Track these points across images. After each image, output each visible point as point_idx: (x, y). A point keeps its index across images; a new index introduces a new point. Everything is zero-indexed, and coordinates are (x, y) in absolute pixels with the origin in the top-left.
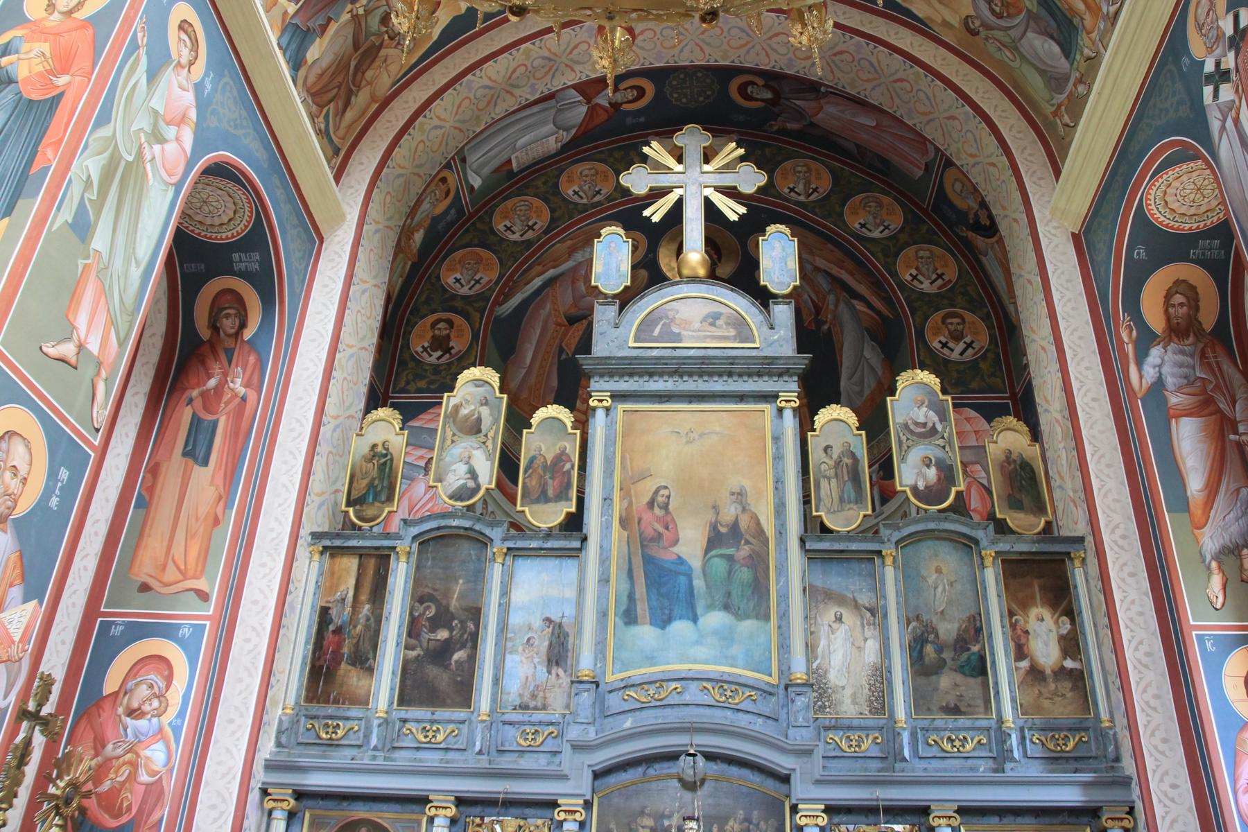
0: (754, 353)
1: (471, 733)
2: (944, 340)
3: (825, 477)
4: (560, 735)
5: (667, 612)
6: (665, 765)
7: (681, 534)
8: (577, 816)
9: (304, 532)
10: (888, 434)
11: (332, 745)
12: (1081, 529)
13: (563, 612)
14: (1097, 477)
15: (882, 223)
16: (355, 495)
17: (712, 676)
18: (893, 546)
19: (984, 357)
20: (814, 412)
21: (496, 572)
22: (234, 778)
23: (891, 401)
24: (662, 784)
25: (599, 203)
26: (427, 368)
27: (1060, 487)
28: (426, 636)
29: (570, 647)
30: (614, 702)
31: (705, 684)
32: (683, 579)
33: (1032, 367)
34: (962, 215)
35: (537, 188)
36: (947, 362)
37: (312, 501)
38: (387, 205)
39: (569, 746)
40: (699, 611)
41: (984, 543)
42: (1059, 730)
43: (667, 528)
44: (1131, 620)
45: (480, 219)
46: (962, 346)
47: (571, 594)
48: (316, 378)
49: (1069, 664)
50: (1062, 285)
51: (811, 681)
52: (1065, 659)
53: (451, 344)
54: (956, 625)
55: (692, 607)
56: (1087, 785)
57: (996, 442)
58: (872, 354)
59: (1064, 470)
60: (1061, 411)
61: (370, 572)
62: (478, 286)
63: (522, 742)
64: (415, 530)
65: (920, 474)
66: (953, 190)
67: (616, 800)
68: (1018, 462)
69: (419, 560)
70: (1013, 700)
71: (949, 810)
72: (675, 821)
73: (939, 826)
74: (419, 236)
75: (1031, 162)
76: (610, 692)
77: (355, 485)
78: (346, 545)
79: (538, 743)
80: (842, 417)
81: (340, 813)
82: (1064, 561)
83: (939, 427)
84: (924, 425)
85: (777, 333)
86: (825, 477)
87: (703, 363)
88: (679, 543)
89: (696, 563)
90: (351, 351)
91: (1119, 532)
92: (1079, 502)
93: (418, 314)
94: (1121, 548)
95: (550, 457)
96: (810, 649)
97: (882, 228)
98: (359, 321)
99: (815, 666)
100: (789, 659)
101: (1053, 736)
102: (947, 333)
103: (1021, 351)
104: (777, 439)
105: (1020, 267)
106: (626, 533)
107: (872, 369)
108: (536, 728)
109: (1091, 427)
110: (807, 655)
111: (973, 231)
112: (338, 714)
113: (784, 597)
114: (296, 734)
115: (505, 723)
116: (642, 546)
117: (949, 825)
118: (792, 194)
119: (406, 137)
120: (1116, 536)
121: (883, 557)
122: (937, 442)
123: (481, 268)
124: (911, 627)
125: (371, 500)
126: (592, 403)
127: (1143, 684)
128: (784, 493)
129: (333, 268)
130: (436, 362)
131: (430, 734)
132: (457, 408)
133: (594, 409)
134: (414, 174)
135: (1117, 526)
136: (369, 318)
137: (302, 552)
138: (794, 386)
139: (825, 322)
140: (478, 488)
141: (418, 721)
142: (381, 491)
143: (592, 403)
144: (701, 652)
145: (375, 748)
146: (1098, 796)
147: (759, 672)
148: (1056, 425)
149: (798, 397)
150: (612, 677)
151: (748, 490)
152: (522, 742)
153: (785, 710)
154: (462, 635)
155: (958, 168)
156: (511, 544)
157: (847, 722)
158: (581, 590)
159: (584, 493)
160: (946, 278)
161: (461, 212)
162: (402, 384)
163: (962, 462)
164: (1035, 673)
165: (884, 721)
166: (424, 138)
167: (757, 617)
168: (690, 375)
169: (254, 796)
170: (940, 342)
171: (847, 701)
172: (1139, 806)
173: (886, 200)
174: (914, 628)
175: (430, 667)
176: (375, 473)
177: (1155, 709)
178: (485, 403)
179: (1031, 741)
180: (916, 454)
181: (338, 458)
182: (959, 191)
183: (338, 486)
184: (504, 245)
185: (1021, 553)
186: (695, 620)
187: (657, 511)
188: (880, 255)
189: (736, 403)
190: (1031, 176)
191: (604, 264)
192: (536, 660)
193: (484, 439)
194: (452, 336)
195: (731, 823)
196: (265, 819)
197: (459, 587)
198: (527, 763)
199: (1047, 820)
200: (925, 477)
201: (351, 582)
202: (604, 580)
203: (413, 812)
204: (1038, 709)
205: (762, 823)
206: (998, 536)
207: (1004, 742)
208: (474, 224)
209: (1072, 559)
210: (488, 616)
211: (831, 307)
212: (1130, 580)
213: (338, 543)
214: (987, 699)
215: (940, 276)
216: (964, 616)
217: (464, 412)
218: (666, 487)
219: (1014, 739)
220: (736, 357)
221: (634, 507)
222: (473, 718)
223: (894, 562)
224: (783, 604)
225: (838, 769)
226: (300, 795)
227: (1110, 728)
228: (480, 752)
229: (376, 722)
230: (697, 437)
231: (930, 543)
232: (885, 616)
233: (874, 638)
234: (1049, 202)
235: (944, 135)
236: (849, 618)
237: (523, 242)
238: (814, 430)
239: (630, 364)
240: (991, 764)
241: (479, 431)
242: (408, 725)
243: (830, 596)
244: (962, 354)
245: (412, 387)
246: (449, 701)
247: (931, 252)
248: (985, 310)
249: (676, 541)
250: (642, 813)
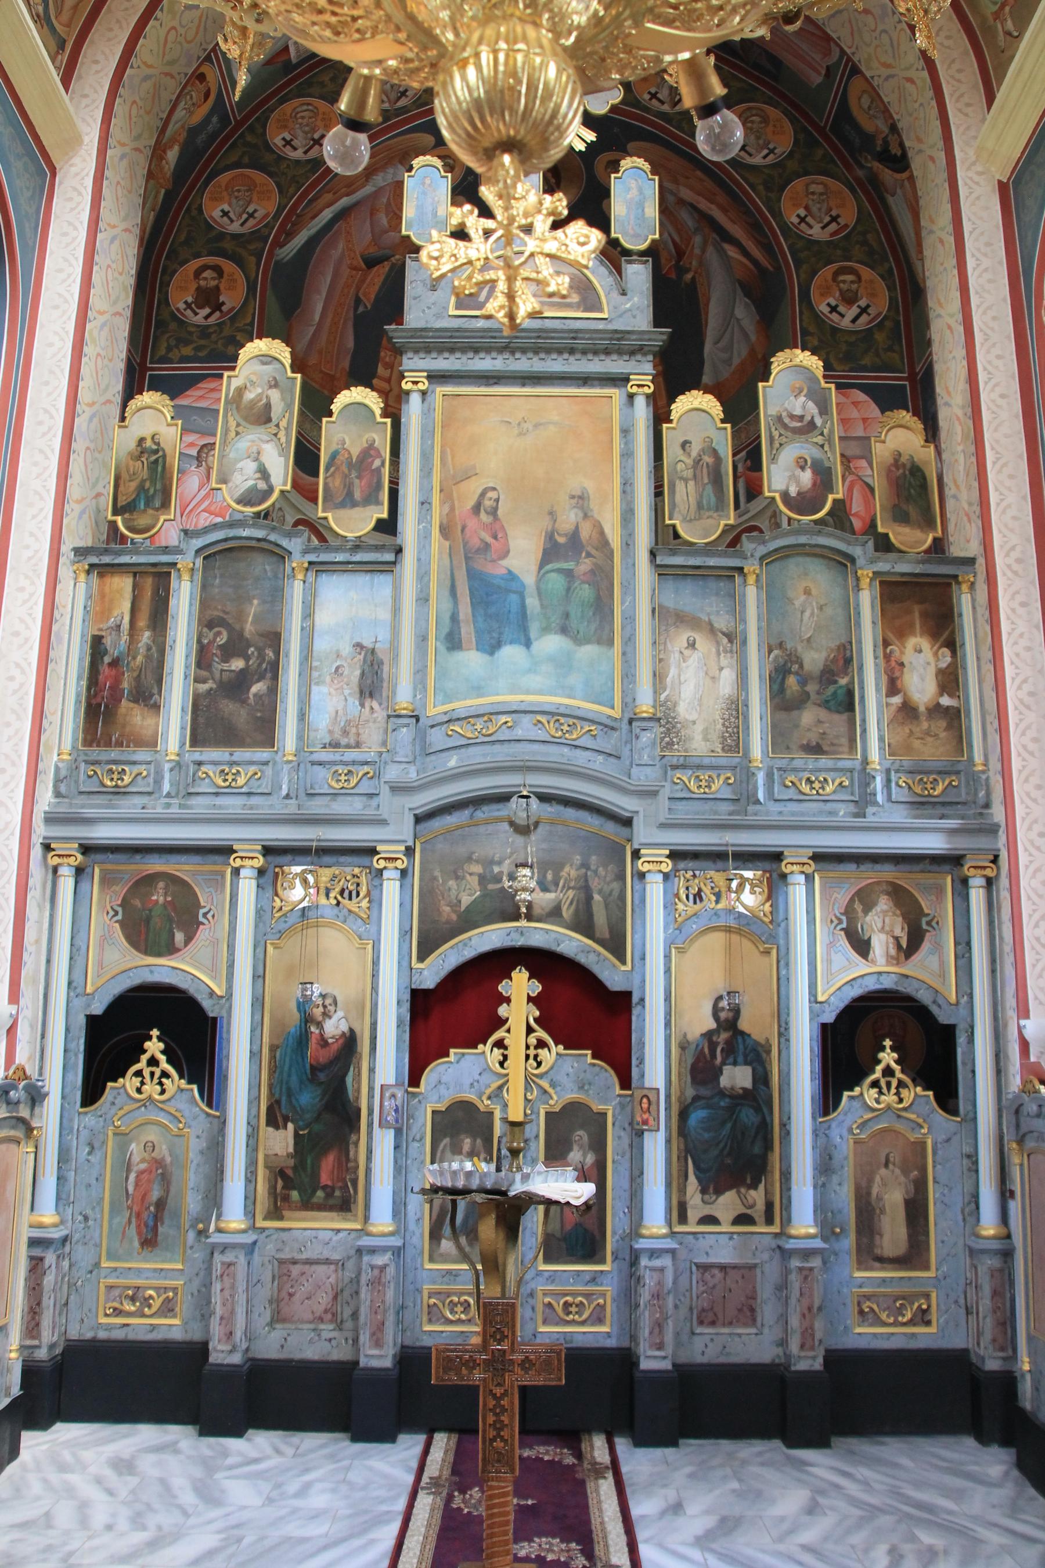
0: (601, 326)
1: (277, 774)
2: (833, 303)
3: (681, 478)
4: (377, 776)
5: (495, 635)
6: (495, 806)
7: (513, 544)
8: (399, 864)
9: (66, 548)
10: (758, 414)
11: (118, 792)
12: (972, 548)
13: (378, 636)
14: (997, 490)
15: (766, 145)
16: (122, 501)
17: (546, 708)
18: (757, 562)
19: (880, 326)
20: (672, 400)
21: (296, 590)
22: (12, 834)
23: (764, 387)
24: (490, 828)
25: (404, 110)
26: (192, 329)
27: (955, 497)
28: (218, 666)
29: (385, 676)
30: (437, 738)
31: (539, 717)
32: (514, 598)
33: (935, 348)
34: (868, 139)
35: (322, 84)
36: (835, 330)
37: (72, 510)
38: (134, 119)
39: (387, 788)
40: (533, 634)
41: (861, 562)
42: (928, 773)
43: (495, 537)
44: (1017, 655)
45: (251, 129)
46: (854, 311)
47: (384, 615)
48: (64, 356)
49: (946, 701)
50: (979, 250)
51: (659, 715)
52: (941, 695)
53: (222, 299)
54: (824, 654)
55: (524, 628)
56: (952, 832)
57: (884, 442)
58: (744, 313)
59: (961, 477)
60: (963, 407)
61: (148, 593)
62: (251, 222)
63: (334, 784)
64: (198, 543)
65: (793, 478)
66: (859, 106)
67: (439, 846)
68: (908, 466)
69: (204, 578)
70: (881, 739)
71: (804, 856)
72: (506, 867)
73: (792, 873)
74: (172, 155)
75: (959, 81)
76: (432, 726)
77: (121, 488)
78: (116, 561)
79: (352, 785)
80: (704, 406)
81: (133, 867)
82: (949, 585)
83: (818, 421)
84: (801, 418)
85: (629, 300)
86: (681, 478)
87: (539, 337)
88: (511, 554)
89: (529, 579)
90: (102, 319)
91: (1014, 555)
92: (973, 517)
93: (176, 259)
94: (1016, 573)
95: (355, 452)
96: (658, 677)
97: (766, 152)
98: (110, 278)
99: (663, 697)
100: (634, 691)
101: (921, 779)
102: (837, 294)
103: (924, 323)
104: (625, 432)
105: (932, 221)
106: (447, 544)
107: (746, 335)
108: (350, 768)
109: (996, 430)
110: (654, 684)
111: (879, 161)
112: (123, 758)
113: (630, 619)
114: (77, 782)
115: (313, 763)
116: (467, 559)
117: (802, 872)
118: (654, 101)
119: (152, 23)
120: (1010, 560)
121: (744, 575)
122: (815, 440)
123: (255, 197)
124: (772, 656)
125: (142, 507)
126: (406, 386)
127: (1022, 726)
128: (633, 497)
129: (72, 209)
130: (203, 322)
131: (230, 777)
132: (240, 391)
133: (408, 393)
134: (166, 74)
135: (1013, 548)
136: (121, 274)
137: (65, 572)
138: (649, 367)
139: (688, 270)
140: (271, 490)
141: (215, 763)
142: (153, 496)
143: (406, 386)
144: (535, 681)
145: (168, 795)
146: (961, 844)
147: (599, 704)
148: (957, 423)
149: (652, 381)
150: (434, 710)
151: (590, 492)
152: (334, 784)
153: (629, 746)
154: (260, 665)
155: (866, 79)
156: (312, 557)
157: (697, 761)
158: (396, 611)
159: (397, 484)
160: (842, 221)
161: (225, 119)
162: (162, 351)
163: (842, 455)
164: (908, 711)
165: (737, 760)
166: (175, 23)
167: (599, 642)
168: (524, 351)
169: (37, 852)
170: (829, 305)
171: (698, 737)
172: (1004, 855)
173: (773, 112)
174: (776, 657)
175: (226, 701)
176: (145, 474)
177: (1032, 754)
178: (275, 384)
179: (898, 785)
180: (790, 453)
181: (97, 455)
182: (866, 107)
183: (99, 488)
184: (283, 166)
185: (903, 574)
186: (528, 644)
187: (484, 517)
188: (761, 188)
189: (579, 386)
190: (957, 101)
191: (418, 207)
192: (347, 692)
193: (274, 430)
194: (222, 287)
195: (567, 869)
196: (50, 876)
197: (254, 608)
198: (341, 807)
199: (907, 867)
200: (798, 482)
201: (126, 606)
202: (423, 599)
203: (215, 863)
204: (908, 749)
205: (601, 869)
206: (878, 554)
207: (868, 784)
208: (242, 135)
209: (959, 583)
210: (289, 642)
211: (697, 251)
212: (1021, 611)
213: (106, 559)
214: (852, 738)
215: (834, 219)
216: (834, 644)
217: (249, 396)
218: (494, 489)
219: (879, 782)
220: (577, 331)
221: (457, 512)
222: (278, 758)
223: (757, 580)
224: (629, 627)
225: (684, 811)
226: (86, 849)
227: (983, 772)
228: (288, 796)
229: (167, 767)
230: (531, 428)
231: (800, 559)
232: (744, 642)
233: (730, 666)
234: (975, 137)
235: (852, 34)
236: (704, 644)
237: (309, 161)
238: (670, 421)
239: (451, 337)
240: (852, 808)
241: (269, 420)
242: (204, 768)
243: (682, 619)
244: (854, 321)
245: (175, 354)
246: (248, 740)
247: (825, 185)
248: (886, 265)
249: (505, 553)
250: (469, 859)
